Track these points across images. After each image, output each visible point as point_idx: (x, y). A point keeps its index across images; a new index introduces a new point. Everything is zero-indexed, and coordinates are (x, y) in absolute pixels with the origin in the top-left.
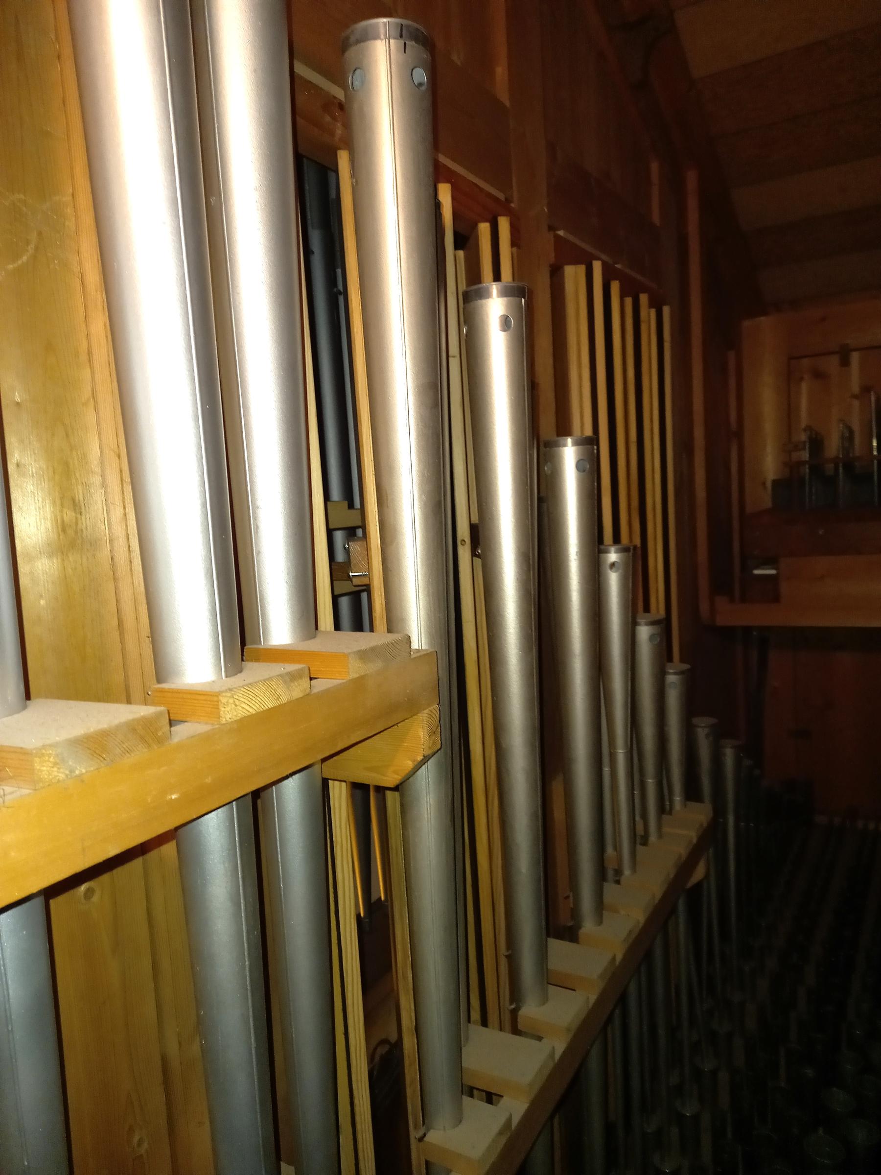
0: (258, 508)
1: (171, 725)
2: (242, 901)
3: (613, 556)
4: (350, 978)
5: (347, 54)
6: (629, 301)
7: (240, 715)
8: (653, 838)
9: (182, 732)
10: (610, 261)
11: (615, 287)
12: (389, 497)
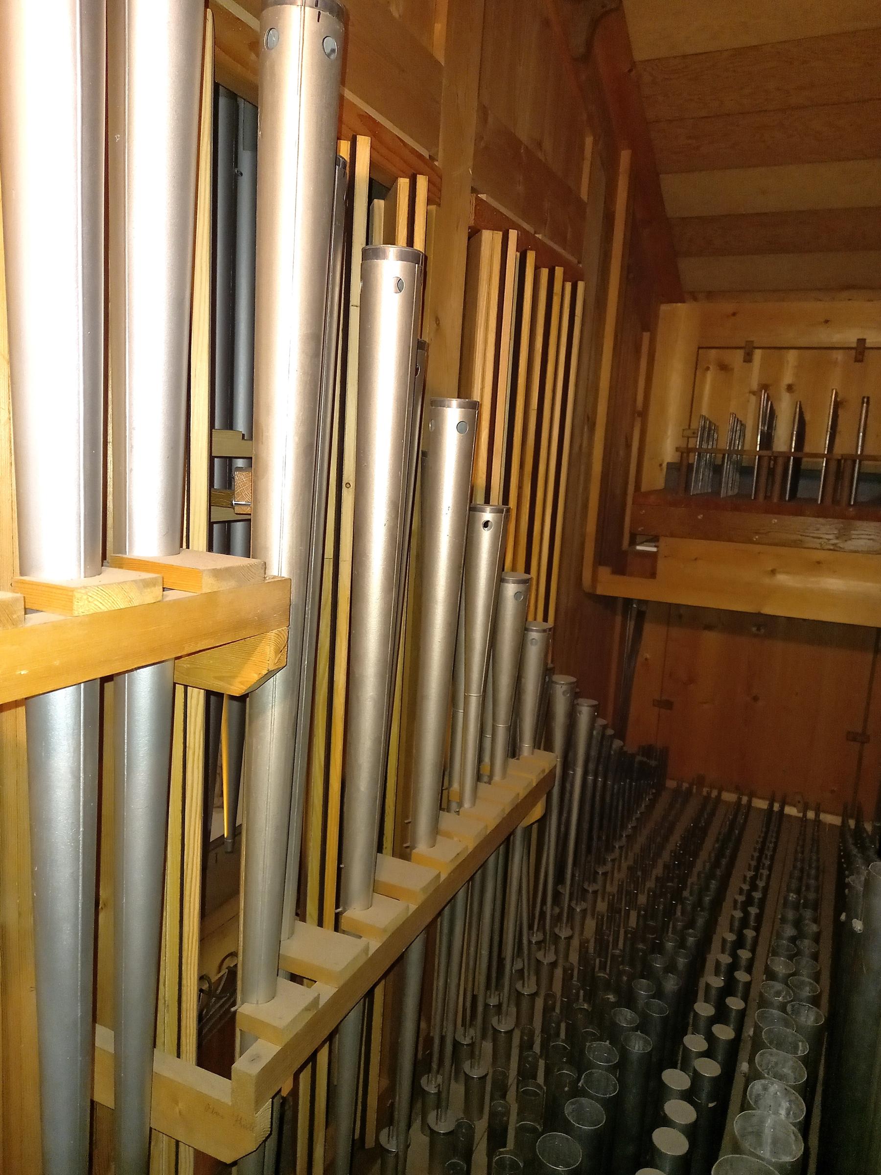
0: (134, 429)
1: (26, 614)
2: (82, 775)
3: (488, 515)
4: (189, 871)
5: (264, 12)
6: (545, 272)
7: (92, 611)
8: (497, 777)
9: (34, 619)
10: (532, 231)
11: (531, 256)
12: (264, 434)
